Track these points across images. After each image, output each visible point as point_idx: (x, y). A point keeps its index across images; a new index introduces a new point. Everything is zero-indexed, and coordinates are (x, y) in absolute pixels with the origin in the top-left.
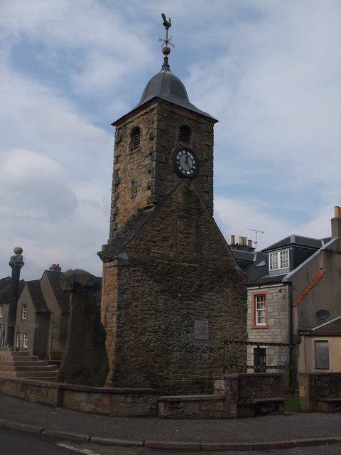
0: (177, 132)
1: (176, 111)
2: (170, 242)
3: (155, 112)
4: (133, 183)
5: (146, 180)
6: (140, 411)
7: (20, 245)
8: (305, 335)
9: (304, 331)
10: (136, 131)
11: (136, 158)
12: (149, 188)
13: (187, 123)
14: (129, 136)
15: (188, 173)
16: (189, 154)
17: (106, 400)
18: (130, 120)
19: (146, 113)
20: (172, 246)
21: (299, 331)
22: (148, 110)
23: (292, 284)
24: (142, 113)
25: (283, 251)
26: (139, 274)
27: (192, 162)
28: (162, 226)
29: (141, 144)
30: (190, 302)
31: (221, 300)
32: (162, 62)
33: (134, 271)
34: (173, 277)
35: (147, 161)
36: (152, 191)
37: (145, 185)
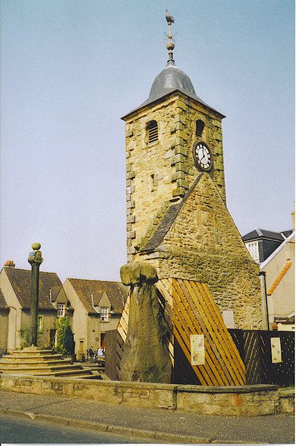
0: (194, 125)
1: (193, 105)
2: (198, 233)
3: (175, 105)
4: (152, 176)
5: (168, 173)
6: (267, 411)
7: (36, 241)
8: (283, 323)
9: (280, 319)
10: (152, 125)
11: (153, 152)
12: (174, 181)
13: (203, 118)
14: (144, 131)
15: (205, 167)
16: (205, 148)
17: (232, 399)
18: (143, 114)
19: (163, 106)
20: (199, 237)
21: (275, 319)
22: (166, 103)
23: (266, 274)
24: (159, 106)
25: (251, 243)
26: (176, 266)
27: (207, 156)
28: (189, 218)
29: (159, 138)
30: (218, 293)
31: (240, 290)
32: (168, 58)
33: (172, 263)
34: (202, 269)
35: (171, 154)
36: (178, 184)
37: (168, 178)
